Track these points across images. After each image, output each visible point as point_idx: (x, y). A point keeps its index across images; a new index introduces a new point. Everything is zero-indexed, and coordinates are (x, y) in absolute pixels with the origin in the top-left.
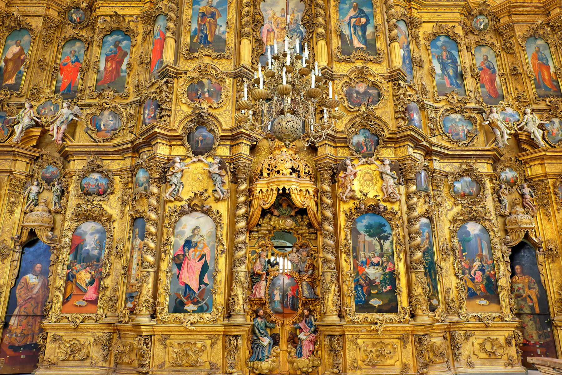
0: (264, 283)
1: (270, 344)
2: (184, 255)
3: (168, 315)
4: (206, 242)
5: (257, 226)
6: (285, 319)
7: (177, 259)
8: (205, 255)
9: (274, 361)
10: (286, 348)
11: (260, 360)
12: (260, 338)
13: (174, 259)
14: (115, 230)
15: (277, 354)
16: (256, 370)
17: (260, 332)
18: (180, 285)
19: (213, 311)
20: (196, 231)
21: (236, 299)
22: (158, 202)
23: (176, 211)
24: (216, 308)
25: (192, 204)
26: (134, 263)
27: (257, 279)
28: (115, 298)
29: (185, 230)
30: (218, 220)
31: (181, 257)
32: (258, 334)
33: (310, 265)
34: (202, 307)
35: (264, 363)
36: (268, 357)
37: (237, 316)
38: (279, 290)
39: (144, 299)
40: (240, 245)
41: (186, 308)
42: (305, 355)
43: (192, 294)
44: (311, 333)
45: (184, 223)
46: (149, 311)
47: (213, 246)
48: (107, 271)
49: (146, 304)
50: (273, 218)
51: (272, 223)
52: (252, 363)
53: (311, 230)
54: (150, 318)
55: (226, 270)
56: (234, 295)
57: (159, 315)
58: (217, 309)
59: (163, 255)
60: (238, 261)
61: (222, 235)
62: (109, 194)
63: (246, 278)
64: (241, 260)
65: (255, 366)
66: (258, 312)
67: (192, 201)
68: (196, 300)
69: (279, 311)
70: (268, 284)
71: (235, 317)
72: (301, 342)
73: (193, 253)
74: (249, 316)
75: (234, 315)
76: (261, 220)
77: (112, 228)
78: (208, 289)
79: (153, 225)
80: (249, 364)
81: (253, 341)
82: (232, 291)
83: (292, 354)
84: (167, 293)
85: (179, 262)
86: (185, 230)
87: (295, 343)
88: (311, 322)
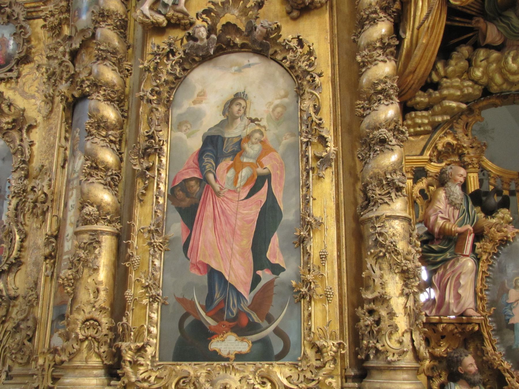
0: (470, 263)
2: (203, 181)
3: (158, 368)
4: (270, 135)
5: (424, 89)
7: (180, 194)
8: (268, 177)
13: (172, 195)
14: (35, 148)
18: (195, 272)
19: (305, 357)
20: (236, 108)
22: (123, 36)
23: (172, 52)
24: (313, 345)
25: (219, 27)
26: (68, 222)
27: (442, 251)
28: (30, 323)
29: (204, 106)
30: (303, 65)
31: (195, 187)
34: (265, 342)
39: (81, 317)
40: (384, 133)
41: (215, 345)
43: (233, 300)
45: (199, 88)
46: (99, 355)
47: (292, 147)
48: (15, 254)
49: (91, 332)
50: (482, 53)
51: (478, 73)
54: (104, 379)
55: (338, 221)
57: (128, 369)
58: (319, 351)
59: (140, 186)
60: (380, 185)
61: (317, 110)
62: (17, 64)
64: (391, 184)
66: (459, 362)
67: (218, 16)
68: (244, 321)
73: (231, 173)
75: (380, 370)
76: (440, 66)
77: (26, 144)
78: (283, 284)
79: (109, 100)
82: (367, 288)
84: (154, 299)
85: (186, 203)
86: (204, 106)
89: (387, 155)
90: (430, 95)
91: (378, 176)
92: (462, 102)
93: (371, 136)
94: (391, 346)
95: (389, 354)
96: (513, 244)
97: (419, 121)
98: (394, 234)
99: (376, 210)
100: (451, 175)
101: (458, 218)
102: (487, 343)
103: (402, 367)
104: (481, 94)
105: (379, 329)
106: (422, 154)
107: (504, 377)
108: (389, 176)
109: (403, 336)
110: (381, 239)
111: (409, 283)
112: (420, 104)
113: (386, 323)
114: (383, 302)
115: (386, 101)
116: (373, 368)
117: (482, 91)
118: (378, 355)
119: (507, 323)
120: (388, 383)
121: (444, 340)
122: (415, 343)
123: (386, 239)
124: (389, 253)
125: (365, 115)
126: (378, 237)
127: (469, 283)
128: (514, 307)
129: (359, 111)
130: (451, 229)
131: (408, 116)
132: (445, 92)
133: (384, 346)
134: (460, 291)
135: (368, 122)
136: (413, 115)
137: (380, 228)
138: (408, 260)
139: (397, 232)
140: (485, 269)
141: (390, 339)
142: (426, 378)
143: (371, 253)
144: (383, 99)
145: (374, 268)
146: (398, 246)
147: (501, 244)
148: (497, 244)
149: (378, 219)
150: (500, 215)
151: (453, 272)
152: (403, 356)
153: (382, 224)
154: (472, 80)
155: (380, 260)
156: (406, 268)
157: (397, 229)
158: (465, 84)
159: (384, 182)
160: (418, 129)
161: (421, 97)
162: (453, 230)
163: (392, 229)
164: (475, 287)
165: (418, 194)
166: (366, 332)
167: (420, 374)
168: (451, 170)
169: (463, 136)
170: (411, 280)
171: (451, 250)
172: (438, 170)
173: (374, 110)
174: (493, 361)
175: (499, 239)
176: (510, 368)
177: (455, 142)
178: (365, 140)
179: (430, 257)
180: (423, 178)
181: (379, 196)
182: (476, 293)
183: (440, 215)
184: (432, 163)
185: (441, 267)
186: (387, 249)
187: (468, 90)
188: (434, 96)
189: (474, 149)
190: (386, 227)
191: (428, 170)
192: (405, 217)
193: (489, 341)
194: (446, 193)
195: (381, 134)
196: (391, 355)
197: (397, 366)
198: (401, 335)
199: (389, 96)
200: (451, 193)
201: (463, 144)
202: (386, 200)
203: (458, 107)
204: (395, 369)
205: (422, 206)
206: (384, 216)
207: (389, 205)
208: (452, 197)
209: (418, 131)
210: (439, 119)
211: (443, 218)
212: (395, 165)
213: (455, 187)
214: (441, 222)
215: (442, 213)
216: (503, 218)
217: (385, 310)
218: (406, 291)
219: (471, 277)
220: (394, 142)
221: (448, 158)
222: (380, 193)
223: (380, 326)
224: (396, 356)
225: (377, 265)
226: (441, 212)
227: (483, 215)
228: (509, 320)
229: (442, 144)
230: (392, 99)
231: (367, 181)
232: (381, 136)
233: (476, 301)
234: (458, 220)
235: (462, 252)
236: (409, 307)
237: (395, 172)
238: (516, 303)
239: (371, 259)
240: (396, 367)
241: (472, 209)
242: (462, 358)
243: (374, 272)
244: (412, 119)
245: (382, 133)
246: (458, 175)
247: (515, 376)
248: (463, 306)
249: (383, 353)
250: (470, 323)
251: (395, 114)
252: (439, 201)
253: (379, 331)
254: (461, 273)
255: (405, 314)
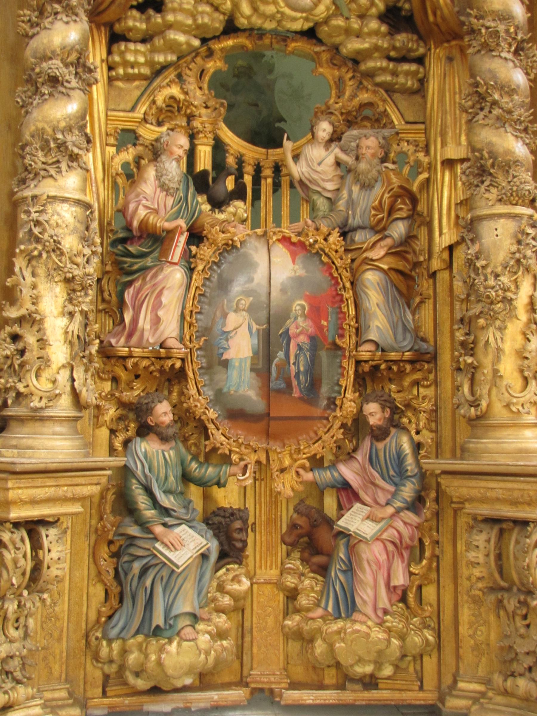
1: (204, 556)
6: (276, 446)
9: (221, 635)
10: (274, 573)
11: (157, 632)
12: (158, 529)
15: (235, 597)
16: (137, 674)
17: (155, 503)
21: (31, 339)
27: (143, 256)
32: (150, 513)
33: (395, 197)
35: (173, 648)
36: (195, 618)
37: (38, 426)
38: (251, 310)
42: (369, 610)
44: (398, 511)
52: (116, 646)
53: (401, 39)
56: (21, 320)
60: (45, 148)
63: (85, 240)
64: (62, 146)
65: (133, 658)
66: (149, 411)
69: (249, 409)
70: (197, 279)
71: (28, 428)
72: (351, 549)
74: (104, 433)
75: (21, 420)
80: (104, 651)
81: (120, 541)
83: (303, 601)
87: (318, 552)
88: (400, 458)
89: (59, 102)
90: (148, 19)
91: (43, 134)
92: (195, 37)
93: (37, 70)
94: (38, 386)
95: (33, 398)
96: (242, 250)
97: (131, 58)
98: (57, 224)
99: (35, 186)
100: (167, 145)
101: (172, 208)
102: (191, 385)
103: (52, 417)
104: (221, 29)
105: (22, 362)
106: (133, 109)
107: (206, 429)
108: (60, 136)
109: (58, 373)
110: (36, 231)
111: (74, 297)
112: (134, 31)
113: (34, 353)
114: (33, 323)
115: (67, 16)
116: (11, 417)
117: (224, 24)
118: (21, 399)
119: (220, 359)
120: (29, 438)
121: (138, 380)
122: (76, 384)
123: (44, 230)
124: (48, 252)
125: (30, 34)
126: (33, 227)
127: (174, 302)
128: (231, 337)
129: (22, 27)
130: (156, 224)
131: (115, 48)
132: (170, 18)
133: (28, 386)
134: (160, 313)
135: (35, 46)
136: (123, 48)
137: (37, 214)
138: (76, 264)
139: (63, 222)
140: (200, 283)
141: (37, 376)
142: (108, 432)
143: (21, 251)
144: (62, 13)
145: (25, 273)
146: (63, 243)
147: (225, 250)
148: (219, 250)
149: (35, 200)
150: (231, 209)
151: (154, 285)
152: (54, 401)
153: (42, 208)
154: (212, 5)
155: (34, 263)
156: (71, 275)
157: (64, 217)
158: (200, 9)
159: (52, 145)
160: (130, 71)
161: (135, 20)
162: (158, 225)
163: (56, 217)
164: (184, 308)
165: (120, 169)
166: (6, 366)
167: (100, 427)
168: (168, 137)
169: (195, 89)
170: (78, 293)
171: (156, 254)
172: (155, 136)
173: (46, 28)
174: (194, 409)
175: (223, 242)
176: (217, 418)
177: (182, 97)
178: (30, 76)
179: (125, 262)
180: (129, 146)
181: (44, 166)
182: (183, 317)
183: (144, 202)
184: (148, 126)
185: (139, 277)
186: (45, 246)
187: (202, 18)
188: (153, 20)
189: (209, 111)
190: (46, 213)
191: (140, 136)
192: (79, 200)
193: (193, 382)
194: (156, 170)
195: (50, 68)
196: (38, 399)
197: (45, 415)
198: (55, 371)
199: (72, 9)
200: (164, 172)
201: (192, 100)
202: (52, 172)
203: (188, 44)
204: (42, 419)
205: (124, 188)
206: (45, 197)
207: (56, 180)
208: (164, 177)
209: (130, 74)
210: (160, 58)
211: (146, 207)
212: (70, 120)
213: (171, 163)
214: (142, 213)
215: (147, 200)
216: (235, 215)
217: (34, 335)
218: (71, 308)
219: (178, 293)
220: (74, 83)
221: (172, 119)
222: (43, 160)
223: (25, 358)
224: (44, 401)
225: (30, 270)
226: (145, 198)
227: (209, 207)
228: (222, 354)
229: (163, 97)
230: (77, 15)
231: (26, 140)
232: (50, 71)
233: (182, 328)
234: (171, 212)
235: (167, 257)
236: (70, 333)
237: (70, 131)
238: (235, 332)
239: (21, 259)
240: (44, 417)
241: (194, 197)
242: (153, 405)
243: (24, 279)
244: (122, 54)
245: (52, 66)
246: (176, 146)
247: (220, 427)
248: (162, 333)
249: (26, 396)
250: (169, 358)
251: (79, 40)
252: (146, 182)
253: (22, 366)
254: (163, 288)
255: (65, 342)
